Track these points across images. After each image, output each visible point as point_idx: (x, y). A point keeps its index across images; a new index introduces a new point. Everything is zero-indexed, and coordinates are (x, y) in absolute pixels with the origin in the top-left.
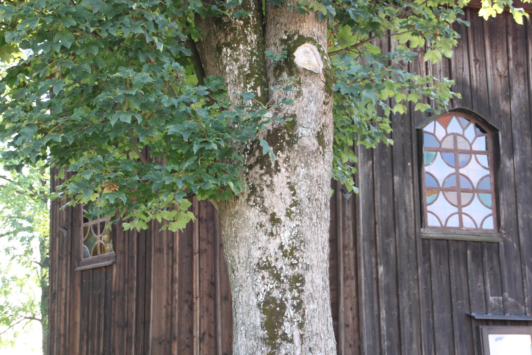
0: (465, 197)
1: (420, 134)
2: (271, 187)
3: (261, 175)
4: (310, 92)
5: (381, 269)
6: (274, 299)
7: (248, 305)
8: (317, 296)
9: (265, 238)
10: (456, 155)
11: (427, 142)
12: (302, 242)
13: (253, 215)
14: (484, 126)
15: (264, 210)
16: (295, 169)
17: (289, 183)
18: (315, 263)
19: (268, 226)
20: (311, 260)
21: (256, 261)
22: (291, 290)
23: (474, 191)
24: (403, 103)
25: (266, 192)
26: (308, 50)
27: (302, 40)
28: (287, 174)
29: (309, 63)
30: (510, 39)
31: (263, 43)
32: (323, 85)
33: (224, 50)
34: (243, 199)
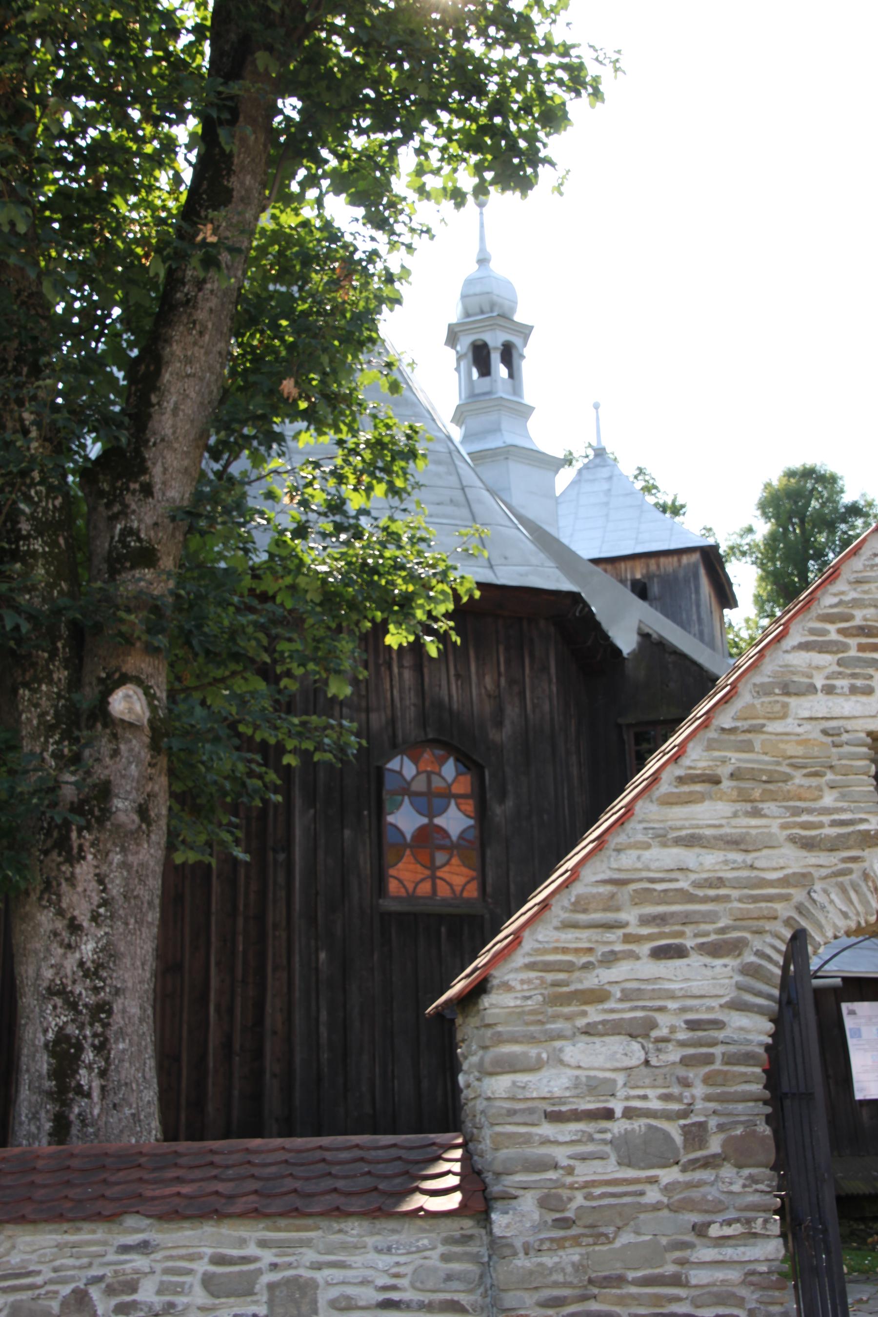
0: (440, 857)
1: (380, 772)
2: (71, 880)
3: (59, 864)
4: (131, 750)
5: (323, 956)
6: (68, 1037)
7: (34, 1045)
8: (129, 1030)
9: (60, 951)
10: (431, 801)
11: (389, 784)
12: (111, 956)
13: (46, 920)
14: (468, 762)
15: (60, 913)
16: (107, 855)
17: (96, 875)
18: (130, 985)
19: (65, 934)
20: (124, 981)
21: (45, 984)
22: (92, 1025)
23: (451, 848)
24: (295, 751)
25: (65, 887)
26: (131, 693)
27: (124, 680)
28: (95, 863)
29: (131, 710)
30: (501, 649)
31: (75, 683)
32: (147, 740)
33: (21, 691)
34: (34, 897)
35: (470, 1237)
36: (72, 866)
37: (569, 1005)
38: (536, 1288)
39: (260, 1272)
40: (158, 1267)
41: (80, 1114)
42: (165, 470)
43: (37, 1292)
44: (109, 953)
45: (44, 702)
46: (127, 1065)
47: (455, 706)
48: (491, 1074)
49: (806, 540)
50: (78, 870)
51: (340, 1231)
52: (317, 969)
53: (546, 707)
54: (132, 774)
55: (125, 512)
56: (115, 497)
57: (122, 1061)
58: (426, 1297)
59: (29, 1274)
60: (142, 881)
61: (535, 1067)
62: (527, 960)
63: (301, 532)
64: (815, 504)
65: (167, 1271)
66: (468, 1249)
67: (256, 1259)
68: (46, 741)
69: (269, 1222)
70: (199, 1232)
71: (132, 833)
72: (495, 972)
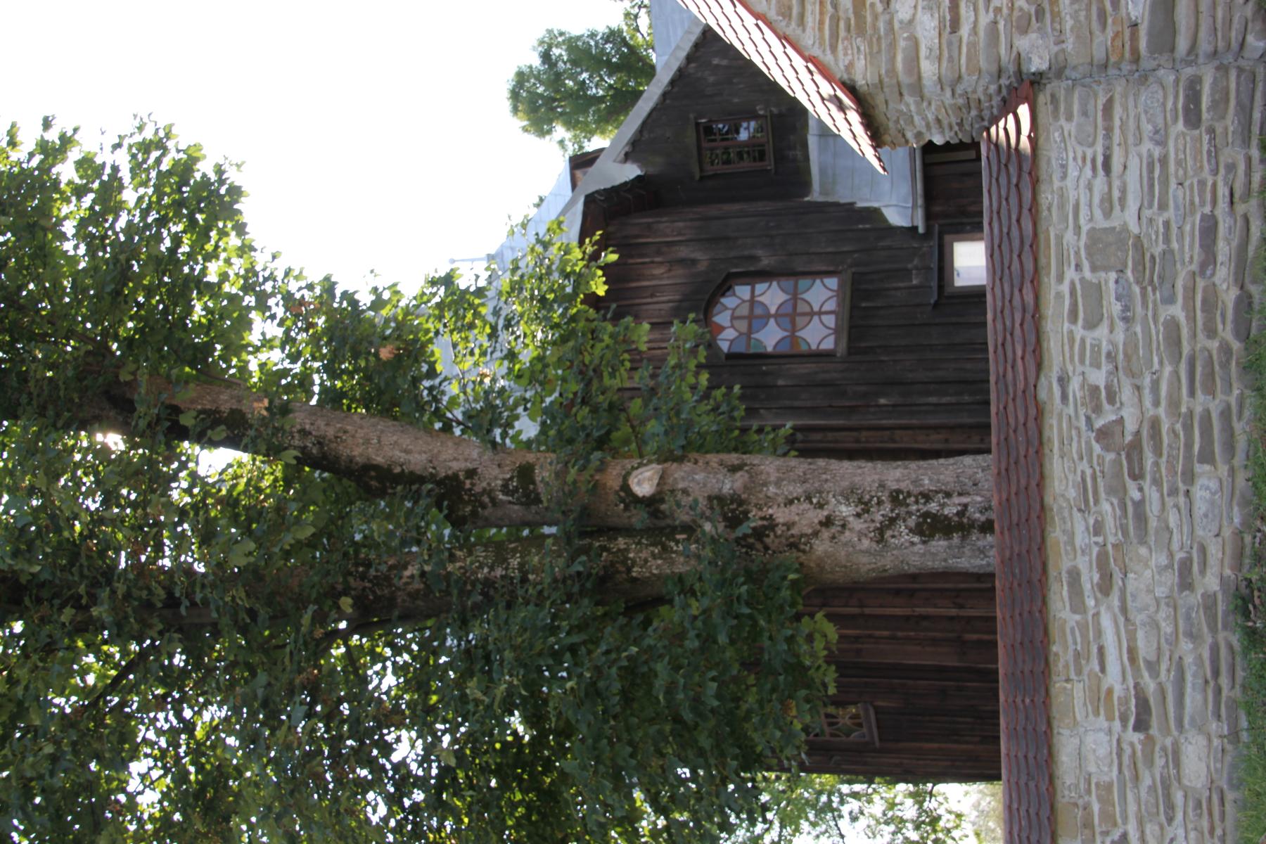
1: (731, 356)
2: (789, 526)
3: (776, 536)
4: (683, 479)
5: (882, 401)
6: (918, 525)
7: (924, 555)
9: (847, 533)
10: (755, 316)
11: (740, 348)
14: (724, 287)
15: (816, 534)
18: (876, 477)
19: (834, 530)
21: (874, 545)
22: (908, 505)
25: (794, 531)
27: (626, 487)
29: (650, 479)
31: (628, 531)
32: (675, 465)
33: (634, 574)
34: (803, 558)
35: (1053, 96)
36: (777, 525)
37: (865, 17)
38: (1091, 33)
39: (1082, 280)
40: (1079, 369)
41: (981, 512)
42: (455, 459)
43: (1098, 474)
44: (850, 494)
45: (643, 555)
46: (942, 477)
47: (677, 297)
48: (920, 78)
49: (570, 95)
50: (781, 520)
51: (1049, 209)
52: (893, 406)
53: (681, 224)
54: (703, 479)
55: (489, 492)
56: (477, 501)
57: (938, 481)
58: (1101, 133)
59: (1084, 480)
60: (792, 469)
61: (915, 43)
62: (828, 52)
63: (512, 356)
64: (541, 90)
65: (1082, 361)
66: (1062, 98)
67: (1072, 284)
68: (675, 552)
69: (1043, 273)
70: (1051, 335)
71: (751, 477)
72: (838, 76)
